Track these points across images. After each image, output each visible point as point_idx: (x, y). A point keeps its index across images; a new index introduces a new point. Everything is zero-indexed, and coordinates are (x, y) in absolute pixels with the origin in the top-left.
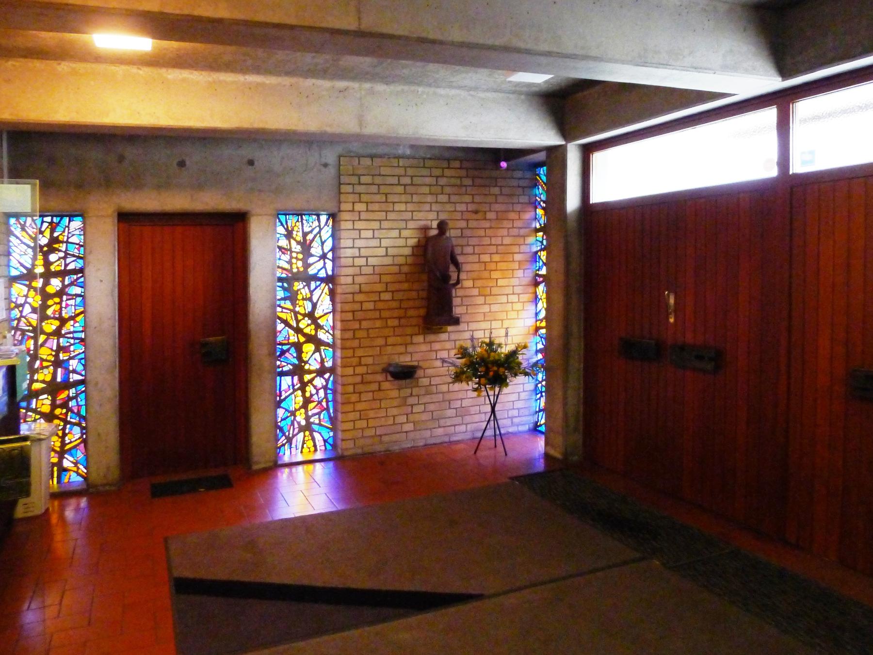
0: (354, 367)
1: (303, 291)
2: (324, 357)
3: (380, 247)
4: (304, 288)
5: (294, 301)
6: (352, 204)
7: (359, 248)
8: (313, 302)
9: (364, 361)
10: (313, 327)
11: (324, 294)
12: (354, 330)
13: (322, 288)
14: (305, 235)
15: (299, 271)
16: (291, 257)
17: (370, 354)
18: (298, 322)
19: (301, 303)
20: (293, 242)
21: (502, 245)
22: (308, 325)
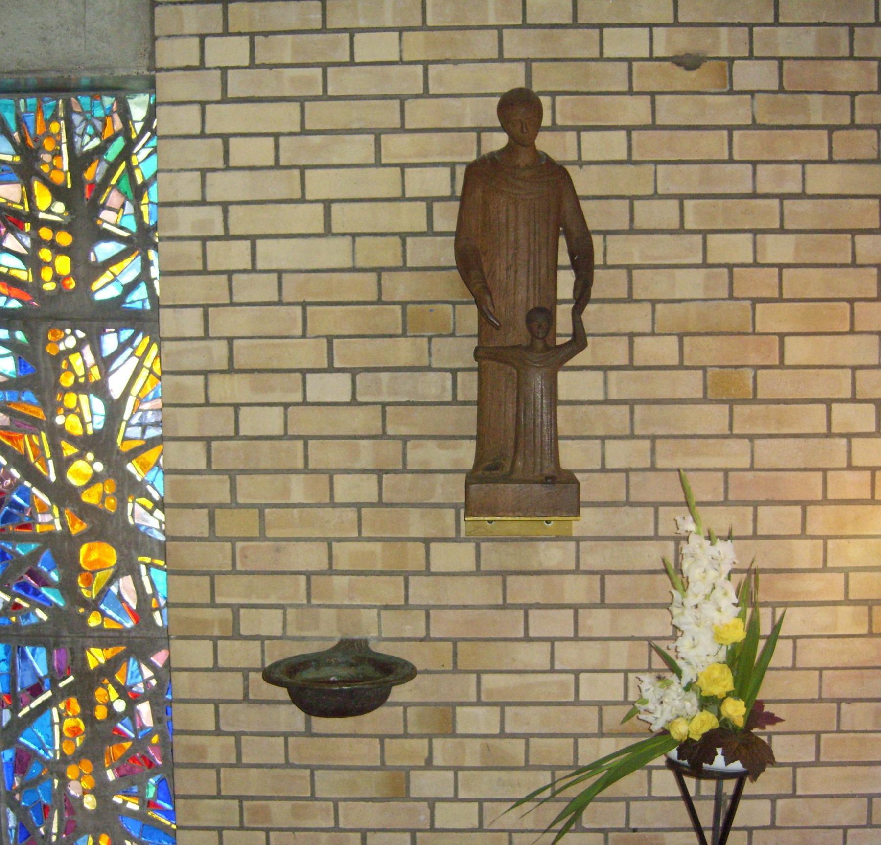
0: (215, 640)
1: (76, 359)
2: (149, 590)
3: (303, 200)
4: (78, 349)
5: (47, 396)
6: (197, 40)
7: (225, 206)
8: (111, 398)
9: (249, 623)
10: (109, 487)
11: (144, 373)
12: (212, 509)
13: (140, 352)
14: (80, 162)
15: (61, 290)
16: (38, 243)
17: (273, 600)
18: (63, 465)
19: (70, 400)
20: (38, 186)
21: (802, 196)
22: (96, 478)
